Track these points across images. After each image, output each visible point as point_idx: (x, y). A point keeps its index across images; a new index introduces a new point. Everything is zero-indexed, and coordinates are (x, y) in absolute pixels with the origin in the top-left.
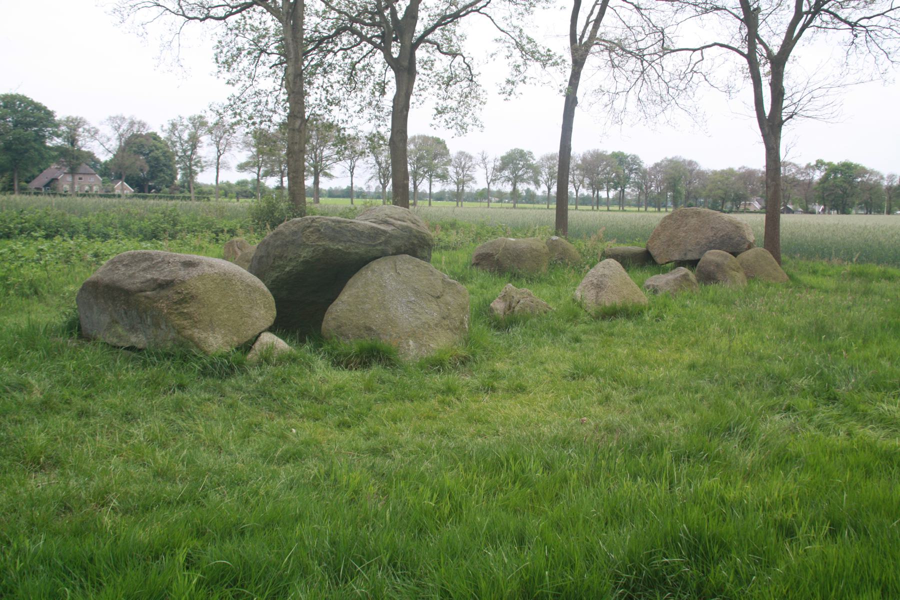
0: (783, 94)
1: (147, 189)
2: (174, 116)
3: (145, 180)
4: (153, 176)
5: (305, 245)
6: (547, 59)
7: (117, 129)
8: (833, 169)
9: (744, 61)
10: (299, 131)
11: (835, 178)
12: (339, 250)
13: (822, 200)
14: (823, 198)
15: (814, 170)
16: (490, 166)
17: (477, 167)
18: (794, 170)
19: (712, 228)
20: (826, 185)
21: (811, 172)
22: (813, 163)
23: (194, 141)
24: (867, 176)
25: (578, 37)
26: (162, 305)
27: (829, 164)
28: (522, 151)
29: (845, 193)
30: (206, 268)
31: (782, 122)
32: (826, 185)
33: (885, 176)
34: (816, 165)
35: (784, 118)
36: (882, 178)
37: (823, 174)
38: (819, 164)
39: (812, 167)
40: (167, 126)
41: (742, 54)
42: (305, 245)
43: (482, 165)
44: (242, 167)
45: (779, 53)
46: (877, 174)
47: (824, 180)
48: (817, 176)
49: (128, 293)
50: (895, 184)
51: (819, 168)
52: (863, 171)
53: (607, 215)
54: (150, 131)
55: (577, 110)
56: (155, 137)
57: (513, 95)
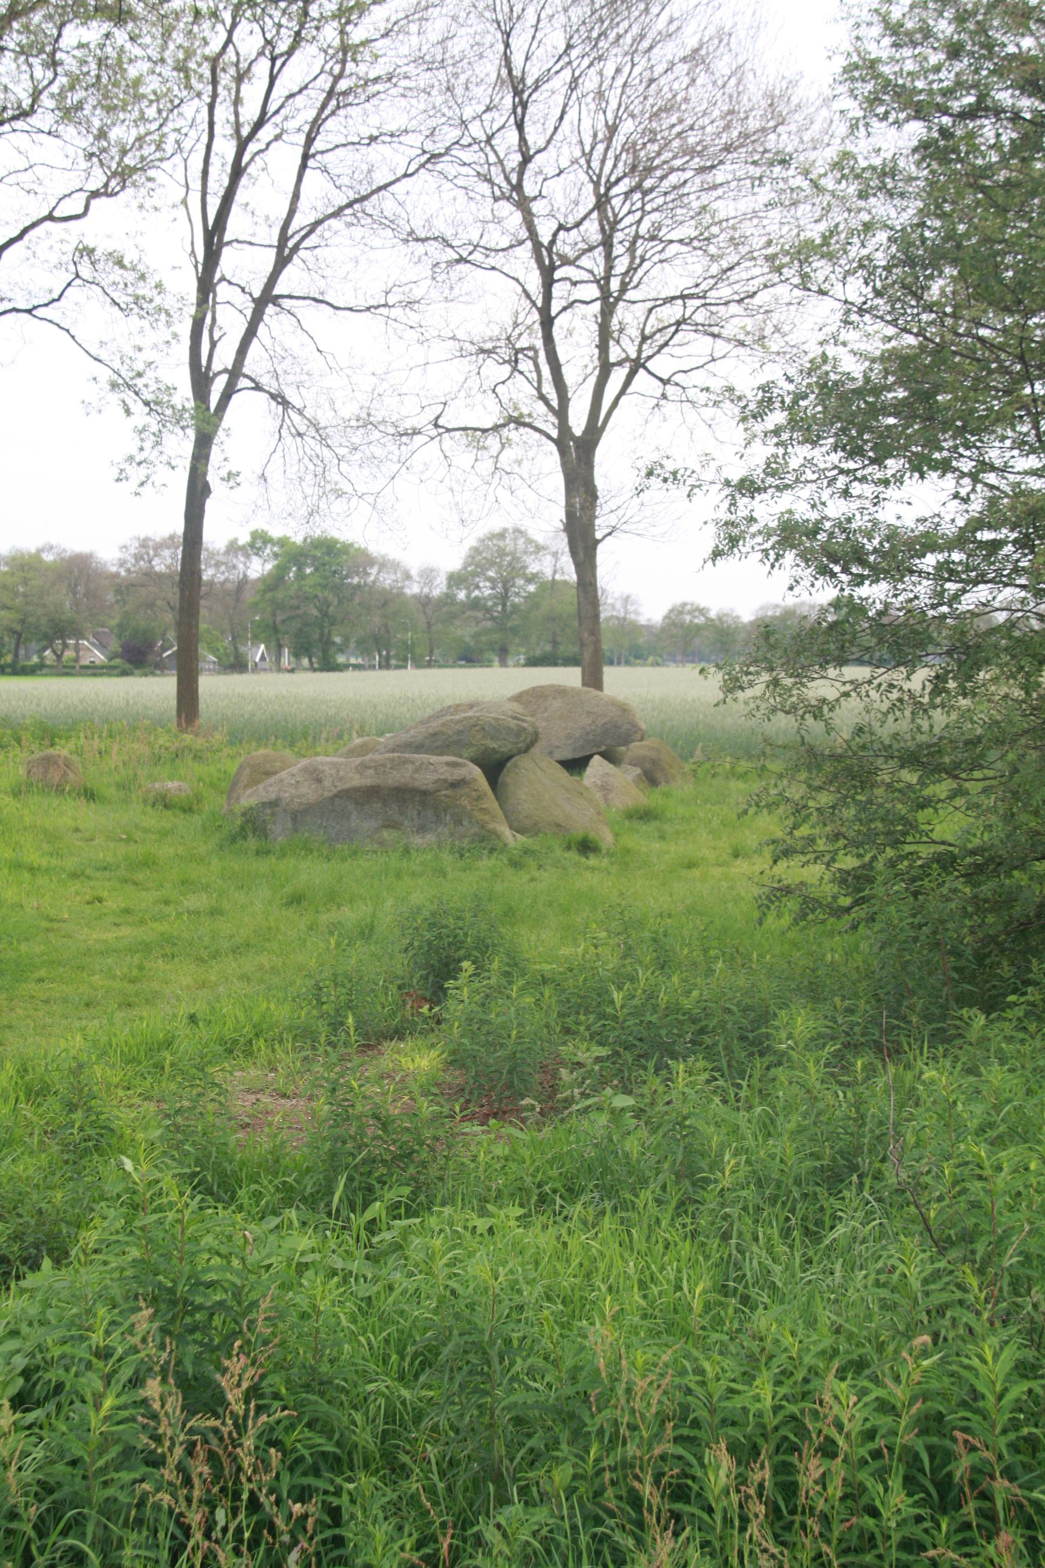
0: (596, 498)
5: (471, 745)
8: (293, 556)
9: (553, 448)
11: (301, 576)
13: (272, 634)
14: (275, 630)
15: (248, 556)
19: (589, 713)
20: (280, 595)
21: (240, 561)
22: (244, 539)
24: (374, 571)
26: (465, 802)
27: (283, 542)
29: (325, 614)
31: (598, 542)
32: (280, 595)
33: (414, 573)
34: (252, 545)
35: (598, 535)
36: (408, 576)
37: (269, 567)
38: (259, 541)
39: (242, 548)
41: (549, 437)
42: (471, 745)
45: (585, 432)
46: (395, 566)
47: (274, 582)
48: (257, 568)
49: (425, 793)
50: (436, 593)
51: (258, 552)
52: (363, 560)
55: (210, 504)
57: (148, 486)
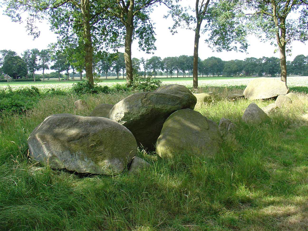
1: (16, 78)
2: (26, 50)
3: (15, 74)
4: (19, 72)
6: (187, 19)
7: (4, 55)
10: (90, 52)
12: (158, 108)
16: (145, 63)
17: (140, 63)
18: (255, 60)
23: (34, 59)
25: (199, 11)
27: (267, 58)
28: (157, 57)
30: (105, 125)
40: (23, 53)
43: (142, 63)
44: (52, 68)
47: (266, 63)
53: (172, 82)
54: (17, 55)
56: (19, 58)
